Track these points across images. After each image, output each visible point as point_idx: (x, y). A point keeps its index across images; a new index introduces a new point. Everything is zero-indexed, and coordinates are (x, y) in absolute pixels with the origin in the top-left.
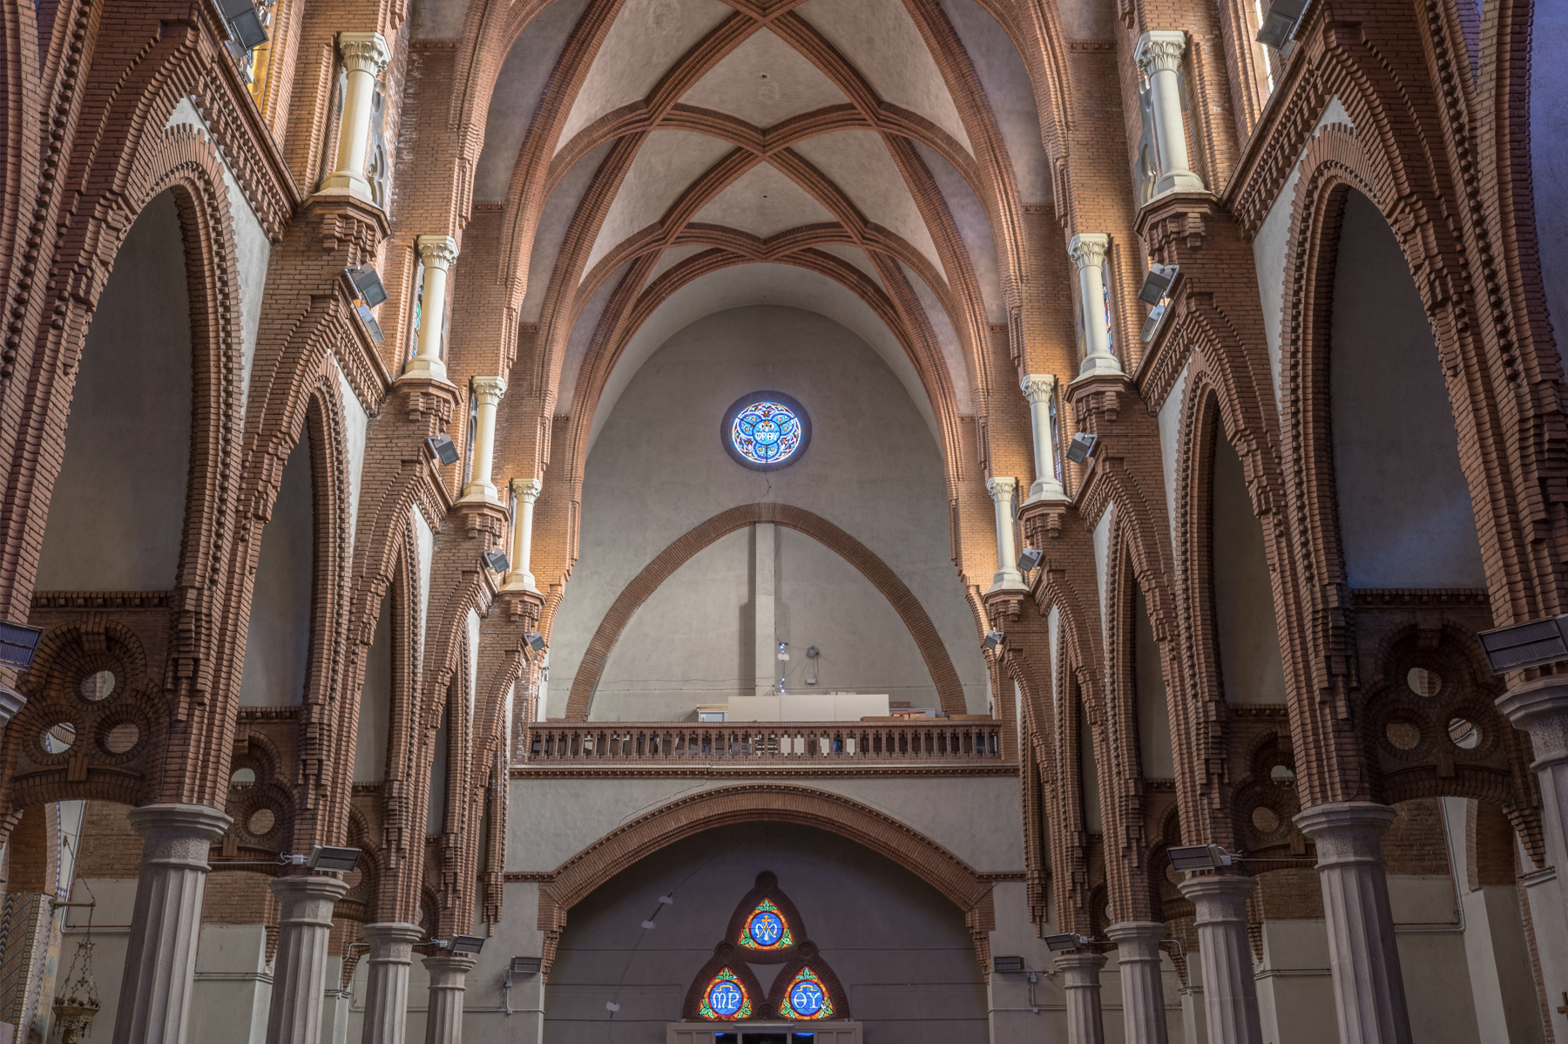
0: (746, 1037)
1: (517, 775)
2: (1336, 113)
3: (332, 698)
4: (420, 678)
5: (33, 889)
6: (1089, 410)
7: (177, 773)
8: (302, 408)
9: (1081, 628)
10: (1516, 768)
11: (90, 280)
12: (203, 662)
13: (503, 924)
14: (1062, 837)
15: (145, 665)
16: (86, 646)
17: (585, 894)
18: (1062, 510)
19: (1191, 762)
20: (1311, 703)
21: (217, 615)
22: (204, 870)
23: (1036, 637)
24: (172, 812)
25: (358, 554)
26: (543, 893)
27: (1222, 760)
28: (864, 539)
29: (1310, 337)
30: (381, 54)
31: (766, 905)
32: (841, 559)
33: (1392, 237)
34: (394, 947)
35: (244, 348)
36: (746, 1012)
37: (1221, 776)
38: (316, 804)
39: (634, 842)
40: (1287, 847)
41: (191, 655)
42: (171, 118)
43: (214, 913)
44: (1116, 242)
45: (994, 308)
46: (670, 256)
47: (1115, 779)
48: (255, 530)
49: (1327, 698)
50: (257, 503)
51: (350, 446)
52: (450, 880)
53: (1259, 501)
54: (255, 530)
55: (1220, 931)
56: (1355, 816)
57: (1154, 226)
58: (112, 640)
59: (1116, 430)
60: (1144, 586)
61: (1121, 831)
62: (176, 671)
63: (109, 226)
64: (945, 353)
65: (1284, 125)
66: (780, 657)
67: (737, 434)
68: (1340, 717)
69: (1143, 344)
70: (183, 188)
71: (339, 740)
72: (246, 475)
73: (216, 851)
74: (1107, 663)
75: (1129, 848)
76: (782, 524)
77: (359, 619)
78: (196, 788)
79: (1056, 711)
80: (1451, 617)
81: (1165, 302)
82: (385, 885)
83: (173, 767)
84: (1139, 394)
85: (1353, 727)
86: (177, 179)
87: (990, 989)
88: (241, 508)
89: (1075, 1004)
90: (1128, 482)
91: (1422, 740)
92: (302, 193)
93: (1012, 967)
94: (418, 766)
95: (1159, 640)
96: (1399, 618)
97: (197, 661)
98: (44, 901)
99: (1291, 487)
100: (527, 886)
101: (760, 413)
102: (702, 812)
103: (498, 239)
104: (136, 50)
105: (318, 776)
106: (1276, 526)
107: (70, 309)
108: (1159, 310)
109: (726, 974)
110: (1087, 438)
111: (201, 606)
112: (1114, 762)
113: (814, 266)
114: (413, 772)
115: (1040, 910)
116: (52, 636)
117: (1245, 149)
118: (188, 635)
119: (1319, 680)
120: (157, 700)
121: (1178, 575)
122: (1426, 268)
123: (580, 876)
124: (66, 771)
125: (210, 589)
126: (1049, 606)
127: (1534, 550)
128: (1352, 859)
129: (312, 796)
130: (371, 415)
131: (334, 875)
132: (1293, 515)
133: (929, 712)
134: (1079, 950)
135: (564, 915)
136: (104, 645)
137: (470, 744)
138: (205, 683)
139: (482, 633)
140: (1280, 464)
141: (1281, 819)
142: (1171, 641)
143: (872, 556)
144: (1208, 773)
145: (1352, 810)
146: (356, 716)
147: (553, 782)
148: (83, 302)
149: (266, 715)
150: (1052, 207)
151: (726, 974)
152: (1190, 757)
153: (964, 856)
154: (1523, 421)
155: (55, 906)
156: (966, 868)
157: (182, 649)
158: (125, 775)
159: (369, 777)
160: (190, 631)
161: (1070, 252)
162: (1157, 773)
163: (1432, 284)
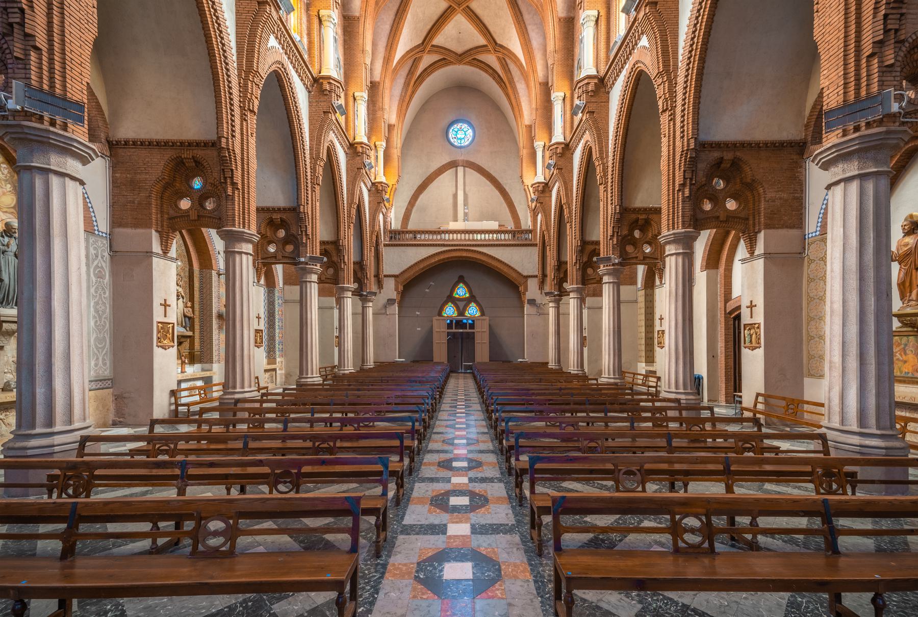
0: (456, 321)
1: (386, 245)
2: (644, 41)
3: (307, 204)
4: (345, 205)
5: (209, 269)
6: (583, 91)
7: (232, 216)
8: (325, 151)
9: (566, 189)
10: (751, 218)
11: (253, 103)
12: (234, 171)
13: (384, 289)
14: (551, 262)
15: (212, 172)
16: (187, 165)
17: (408, 281)
18: (563, 146)
19: (607, 228)
20: (674, 189)
21: (310, 213)
22: (251, 255)
23: (548, 199)
24: (231, 231)
25: (311, 149)
26: (396, 281)
27: (693, 171)
28: (492, 172)
29: (706, 13)
30: (334, 20)
31: (461, 285)
32: (484, 179)
33: (654, 85)
34: (345, 293)
35: (228, 23)
36: (456, 314)
37: (618, 233)
38: (307, 241)
39: (422, 266)
40: (637, 257)
41: (229, 167)
42: (269, 44)
43: (321, 293)
44: (600, 14)
45: (541, 75)
46: (427, 60)
47: (574, 240)
48: (317, 188)
49: (681, 188)
50: (249, 103)
51: (342, 164)
52: (365, 275)
53: (663, 105)
54: (317, 188)
55: (611, 285)
56: (686, 234)
57: (579, 88)
58: (197, 162)
59: (593, 100)
60: (564, 207)
61: (553, 274)
62: (224, 174)
63: (256, 84)
64: (522, 100)
65: (628, 43)
66: (466, 211)
67: (451, 135)
68: (686, 196)
69: (608, 57)
70: (276, 70)
71: (312, 219)
72: (241, 90)
73: (319, 278)
74: (574, 201)
75: (576, 263)
76: (467, 167)
77: (315, 175)
78: (241, 222)
79: (552, 222)
80: (738, 154)
81: (580, 115)
82: (341, 273)
83: (230, 214)
84: (603, 84)
85: (690, 199)
86: (274, 68)
87: (525, 308)
88: (242, 105)
89: (552, 312)
90: (595, 122)
91: (715, 207)
92: (315, 73)
93: (532, 302)
94: (348, 235)
95: (600, 184)
96: (716, 154)
97: (232, 170)
98: (214, 273)
99: (610, 177)
100: (391, 278)
101: (458, 127)
102: (442, 257)
103: (358, 32)
104: (251, 15)
105: (306, 231)
106: (669, 116)
107: (316, 186)
108: (577, 119)
109: (450, 304)
110: (552, 162)
111: (229, 146)
112: (574, 235)
113: (477, 66)
114: (346, 237)
115: (541, 287)
116: (170, 159)
117: (575, 127)
118: (225, 158)
119: (679, 180)
120: (219, 187)
121: (610, 158)
122: (663, 98)
123: (406, 276)
124: (189, 216)
125: (232, 139)
126: (538, 213)
127: (867, 61)
128: (682, 251)
129: (343, 265)
130: (309, 92)
131: (316, 265)
132: (609, 184)
133: (510, 226)
134: (554, 296)
135: (402, 287)
136: (194, 165)
137: (368, 233)
138: (309, 232)
139: (369, 196)
140: (675, 87)
141: (594, 271)
142: (670, 110)
143: (494, 177)
144: (613, 232)
145: (686, 232)
146: (318, 211)
147: (397, 248)
148: (252, 111)
149: (284, 209)
150: (548, 83)
151: (450, 304)
152: (607, 226)
153: (520, 270)
154: (683, 151)
155: (219, 275)
156: (520, 274)
157: (225, 165)
158: (214, 218)
159: (358, 259)
160: (226, 157)
161: (552, 99)
162: (563, 259)
163: (663, 103)
